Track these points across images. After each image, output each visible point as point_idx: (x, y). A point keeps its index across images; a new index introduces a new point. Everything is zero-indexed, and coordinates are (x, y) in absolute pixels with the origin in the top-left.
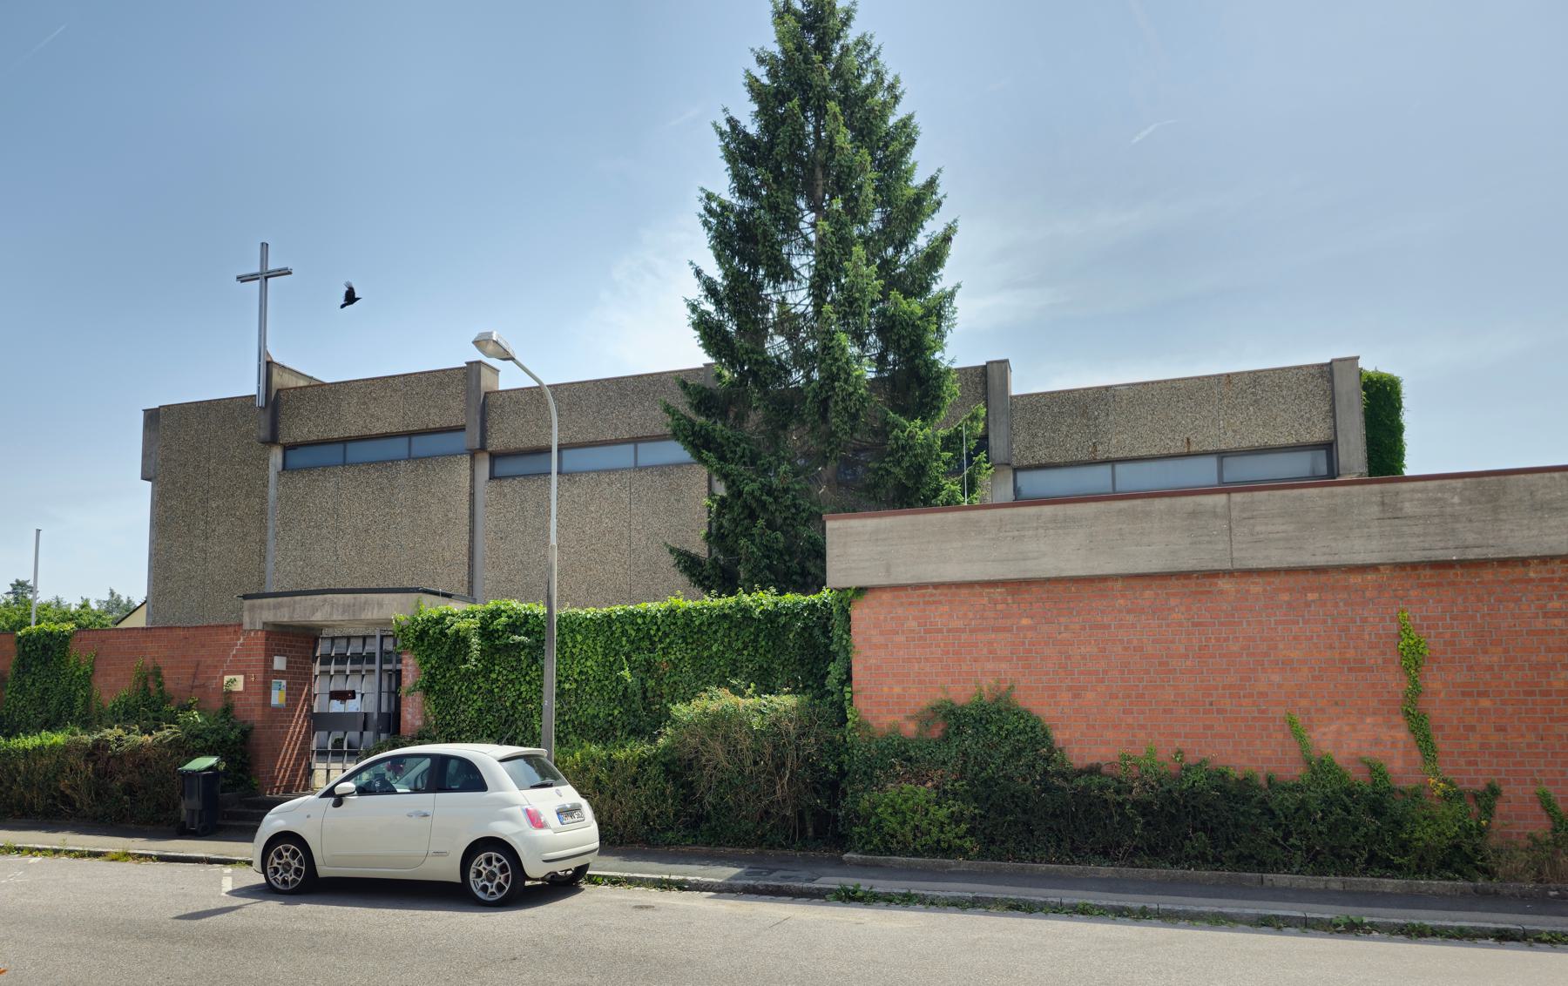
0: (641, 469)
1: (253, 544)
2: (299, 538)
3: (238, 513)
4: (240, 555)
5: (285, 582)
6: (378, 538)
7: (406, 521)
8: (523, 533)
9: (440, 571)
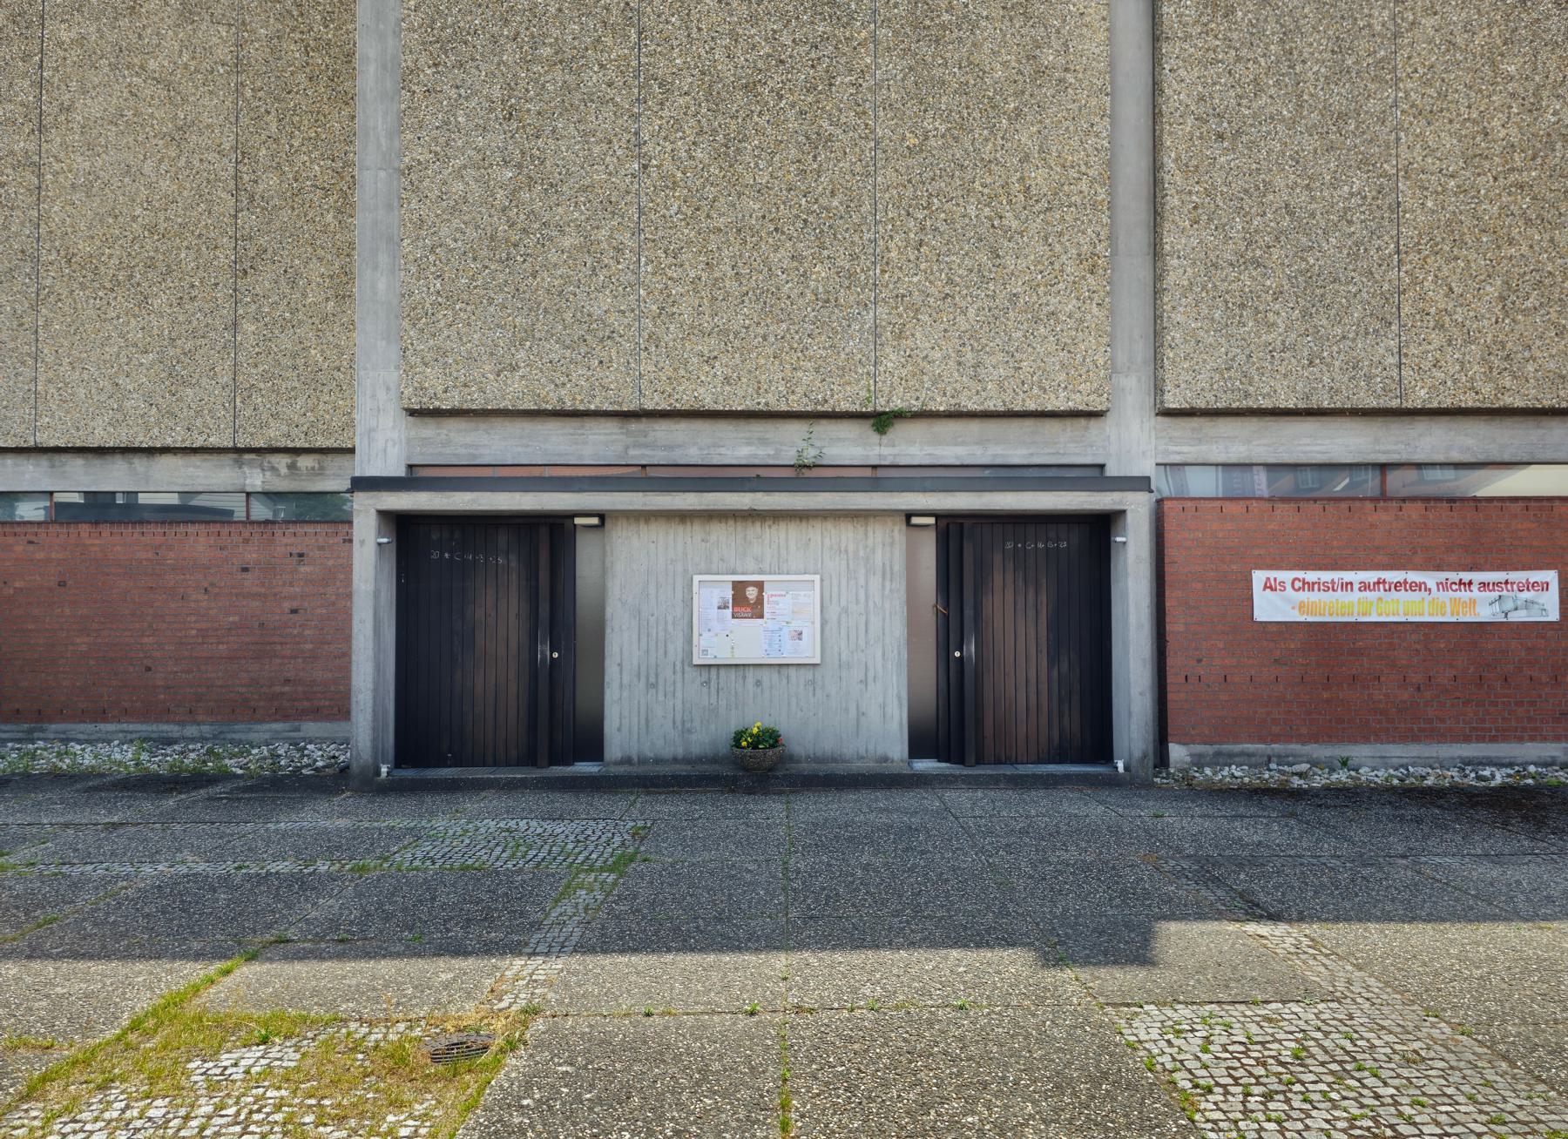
0: (253, 523)
1: (212, 156)
2: (497, 93)
3: (152, 65)
4: (165, 185)
5: (444, 231)
6: (791, 114)
7: (892, 67)
8: (1292, 124)
9: (1015, 224)
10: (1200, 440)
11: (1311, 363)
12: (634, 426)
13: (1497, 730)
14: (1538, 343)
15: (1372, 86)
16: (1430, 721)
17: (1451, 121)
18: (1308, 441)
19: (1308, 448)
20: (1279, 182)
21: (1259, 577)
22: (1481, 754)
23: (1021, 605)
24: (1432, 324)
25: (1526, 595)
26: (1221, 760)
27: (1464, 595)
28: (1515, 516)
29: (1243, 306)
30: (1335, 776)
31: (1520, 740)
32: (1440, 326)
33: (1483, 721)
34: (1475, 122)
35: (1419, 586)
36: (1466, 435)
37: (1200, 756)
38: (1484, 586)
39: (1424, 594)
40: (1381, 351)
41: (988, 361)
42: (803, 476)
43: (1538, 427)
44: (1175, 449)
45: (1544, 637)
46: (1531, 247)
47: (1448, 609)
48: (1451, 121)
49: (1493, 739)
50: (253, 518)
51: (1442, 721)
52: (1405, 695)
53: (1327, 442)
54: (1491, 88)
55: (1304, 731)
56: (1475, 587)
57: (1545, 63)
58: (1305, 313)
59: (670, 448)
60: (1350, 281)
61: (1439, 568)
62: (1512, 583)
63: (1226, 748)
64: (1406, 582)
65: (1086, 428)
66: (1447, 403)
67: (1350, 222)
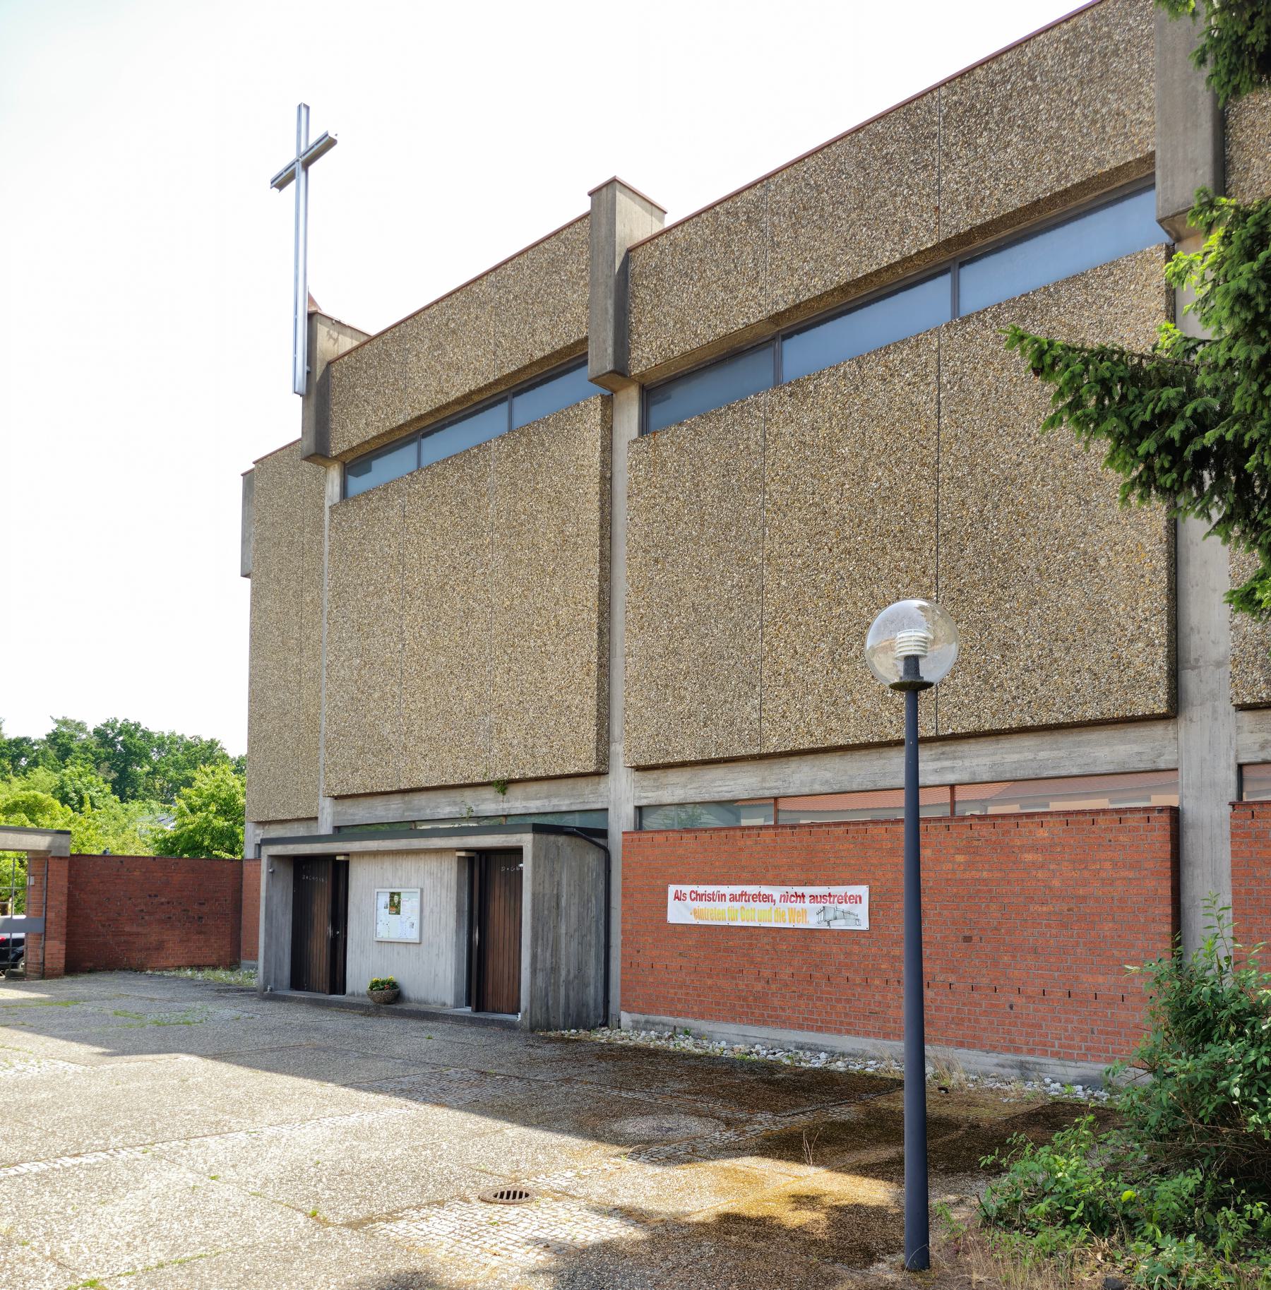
10: (658, 787)
11: (705, 725)
12: (407, 798)
13: (822, 1022)
14: (858, 687)
15: (748, 496)
16: (775, 1009)
17: (800, 509)
18: (720, 783)
19: (720, 789)
20: (689, 588)
21: (672, 889)
22: (810, 1041)
23: (507, 909)
24: (782, 682)
25: (844, 907)
26: (648, 1026)
27: (798, 906)
28: (838, 839)
29: (667, 686)
30: (549, 1033)
31: (839, 1032)
32: (787, 684)
33: (811, 1013)
34: (816, 505)
35: (767, 898)
36: (826, 770)
37: (637, 1022)
38: (813, 897)
39: (771, 904)
40: (749, 709)
41: (539, 743)
42: (407, 828)
43: (881, 758)
44: (645, 795)
45: (858, 943)
46: (855, 603)
47: (787, 917)
48: (800, 509)
49: (819, 1029)
50: (780, 823)
51: (783, 1010)
52: (759, 987)
53: (732, 783)
54: (830, 472)
55: (696, 1009)
56: (807, 899)
57: (871, 437)
58: (703, 686)
59: (419, 810)
60: (731, 656)
61: (783, 883)
62: (835, 896)
63: (652, 1018)
64: (760, 894)
65: (599, 783)
66: (790, 746)
67: (731, 609)
